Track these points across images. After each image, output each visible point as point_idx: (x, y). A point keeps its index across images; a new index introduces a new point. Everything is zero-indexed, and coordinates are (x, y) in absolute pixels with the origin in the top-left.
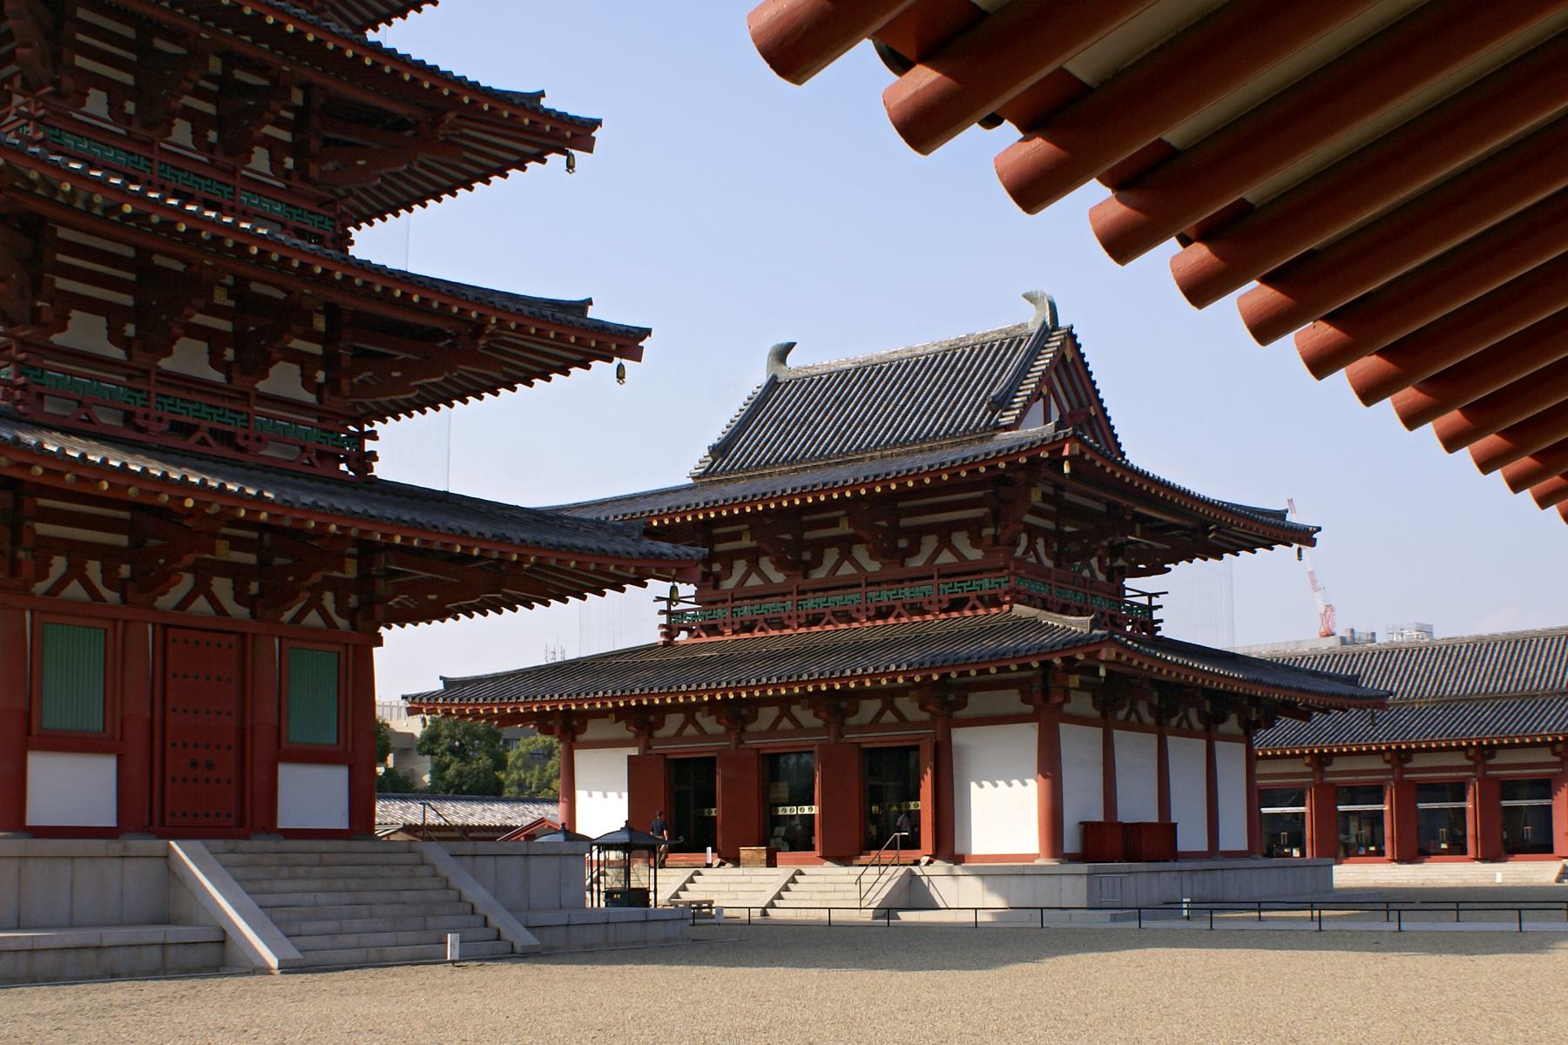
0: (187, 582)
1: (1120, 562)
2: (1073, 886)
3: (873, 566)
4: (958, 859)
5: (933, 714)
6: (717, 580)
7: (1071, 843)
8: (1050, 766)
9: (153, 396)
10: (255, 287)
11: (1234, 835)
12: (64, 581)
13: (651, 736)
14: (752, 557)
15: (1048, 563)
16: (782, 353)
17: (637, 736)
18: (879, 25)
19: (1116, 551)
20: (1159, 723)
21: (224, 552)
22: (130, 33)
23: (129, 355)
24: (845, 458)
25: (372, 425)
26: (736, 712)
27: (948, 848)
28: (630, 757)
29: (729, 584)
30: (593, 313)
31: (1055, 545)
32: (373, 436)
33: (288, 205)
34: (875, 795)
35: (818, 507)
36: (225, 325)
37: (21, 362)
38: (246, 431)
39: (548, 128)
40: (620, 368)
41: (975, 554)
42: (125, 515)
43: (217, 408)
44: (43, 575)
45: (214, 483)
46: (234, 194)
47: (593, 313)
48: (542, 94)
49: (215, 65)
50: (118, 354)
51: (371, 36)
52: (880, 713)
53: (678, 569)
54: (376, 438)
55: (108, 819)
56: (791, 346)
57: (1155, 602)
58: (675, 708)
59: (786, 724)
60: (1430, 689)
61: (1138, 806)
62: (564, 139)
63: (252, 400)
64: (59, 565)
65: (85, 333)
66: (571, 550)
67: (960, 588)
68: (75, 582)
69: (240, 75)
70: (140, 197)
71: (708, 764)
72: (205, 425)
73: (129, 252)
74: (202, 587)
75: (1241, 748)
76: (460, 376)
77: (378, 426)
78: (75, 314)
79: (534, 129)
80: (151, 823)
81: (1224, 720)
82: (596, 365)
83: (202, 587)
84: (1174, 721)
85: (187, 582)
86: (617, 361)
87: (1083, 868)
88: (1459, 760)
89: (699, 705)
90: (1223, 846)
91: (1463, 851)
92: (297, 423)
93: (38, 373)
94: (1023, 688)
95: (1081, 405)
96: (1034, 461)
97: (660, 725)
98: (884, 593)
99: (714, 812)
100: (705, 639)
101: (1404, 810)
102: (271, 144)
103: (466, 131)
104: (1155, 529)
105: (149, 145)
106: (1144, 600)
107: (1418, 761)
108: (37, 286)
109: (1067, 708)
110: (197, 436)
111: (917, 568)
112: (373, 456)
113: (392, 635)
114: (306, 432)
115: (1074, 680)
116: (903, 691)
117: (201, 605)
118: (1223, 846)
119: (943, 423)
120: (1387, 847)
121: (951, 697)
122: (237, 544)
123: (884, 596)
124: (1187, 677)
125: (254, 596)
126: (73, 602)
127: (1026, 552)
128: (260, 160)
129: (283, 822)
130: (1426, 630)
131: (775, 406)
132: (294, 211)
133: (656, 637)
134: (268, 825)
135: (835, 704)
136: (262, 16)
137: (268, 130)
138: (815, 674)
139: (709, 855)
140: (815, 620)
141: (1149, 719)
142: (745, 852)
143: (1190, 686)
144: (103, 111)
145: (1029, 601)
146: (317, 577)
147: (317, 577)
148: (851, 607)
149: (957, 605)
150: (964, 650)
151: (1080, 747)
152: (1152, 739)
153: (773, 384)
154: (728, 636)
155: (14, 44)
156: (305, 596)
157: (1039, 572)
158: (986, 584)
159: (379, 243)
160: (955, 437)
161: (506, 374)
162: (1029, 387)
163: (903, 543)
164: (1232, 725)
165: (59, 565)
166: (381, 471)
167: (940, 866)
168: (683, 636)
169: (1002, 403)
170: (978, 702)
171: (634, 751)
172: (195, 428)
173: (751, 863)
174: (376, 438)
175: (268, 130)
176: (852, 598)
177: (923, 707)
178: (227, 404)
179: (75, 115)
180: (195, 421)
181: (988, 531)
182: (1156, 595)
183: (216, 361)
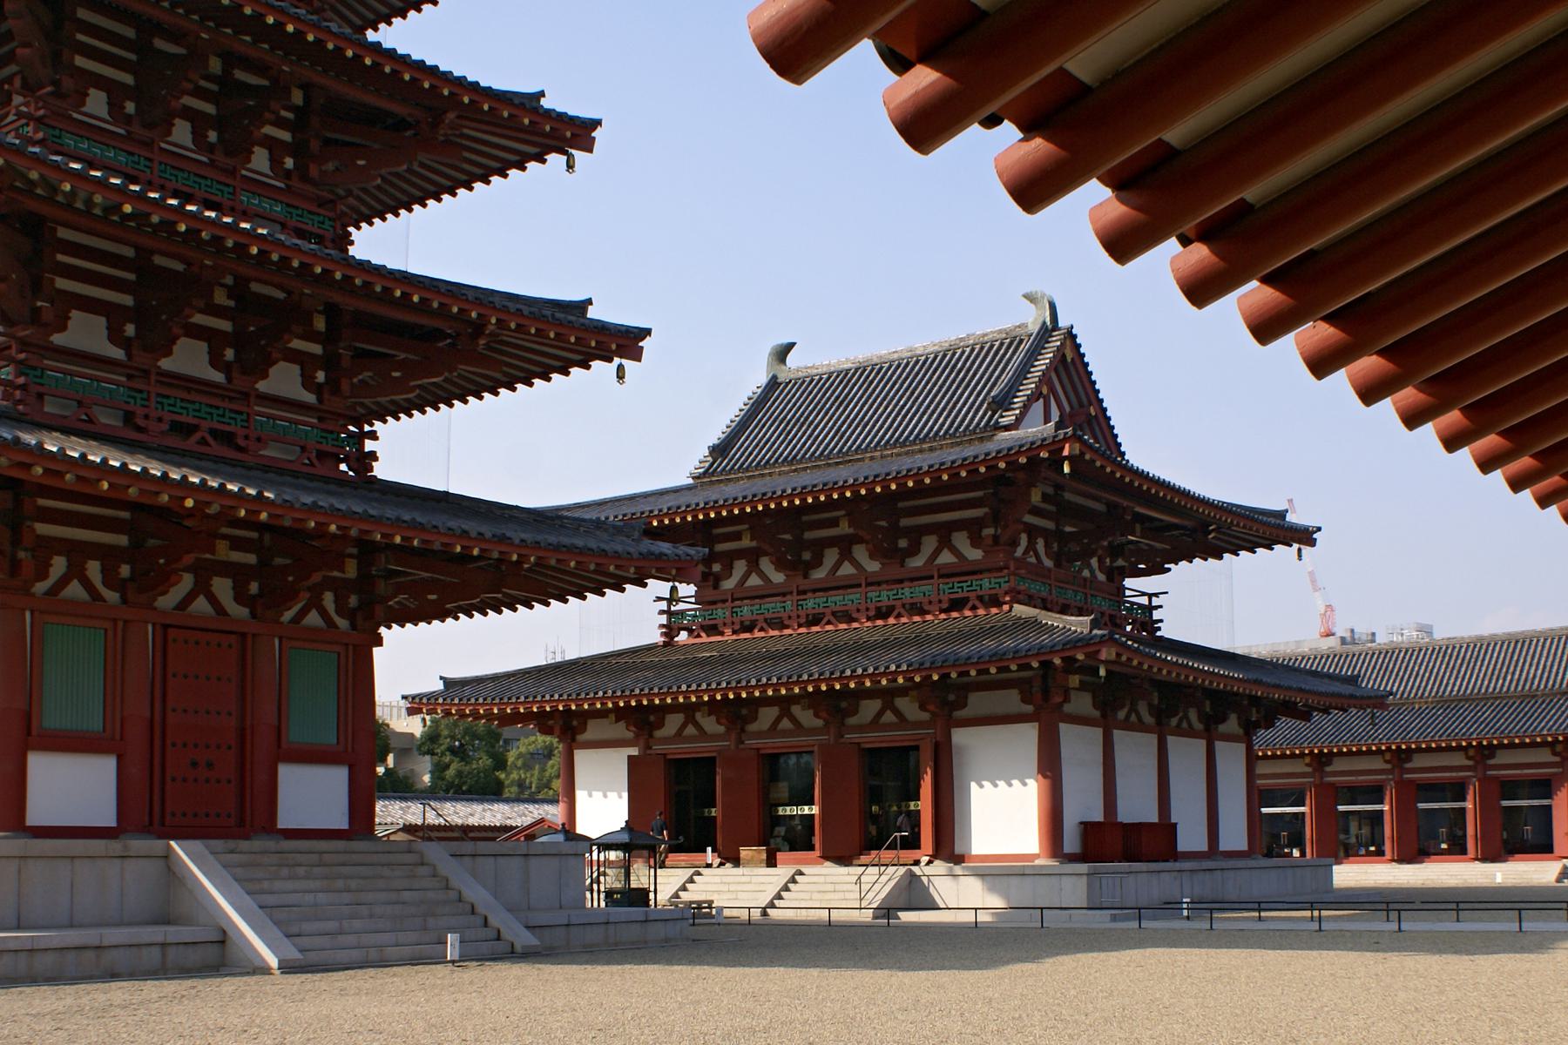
0: (187, 582)
1: (1120, 562)
2: (1073, 886)
3: (873, 566)
4: (958, 859)
5: (933, 714)
6: (717, 580)
7: (1071, 843)
8: (1050, 766)
9: (153, 396)
10: (255, 287)
11: (1234, 835)
12: (64, 581)
13: (651, 736)
14: (752, 557)
15: (1048, 563)
16: (782, 353)
17: (637, 736)
18: (879, 25)
19: (1116, 551)
20: (1159, 723)
21: (224, 552)
22: (130, 33)
23: (129, 355)
24: (845, 458)
25: (372, 425)
26: (736, 712)
27: (948, 848)
28: (630, 757)
29: (729, 584)
30: (593, 313)
31: (1055, 545)
32: (373, 436)
33: (288, 205)
34: (875, 795)
35: (818, 507)
36: (225, 325)
37: (21, 362)
38: (246, 431)
39: (548, 128)
40: (620, 368)
41: (975, 554)
42: (125, 515)
43: (217, 408)
44: (43, 575)
45: (214, 483)
46: (234, 194)
47: (593, 313)
48: (542, 94)
49: (215, 65)
50: (118, 354)
51: (371, 36)
52: (880, 713)
53: (678, 569)
54: (376, 438)
55: (108, 819)
56: (791, 346)
57: (1155, 602)
58: (675, 708)
59: (786, 724)
60: (1430, 689)
61: (1138, 806)
62: (564, 139)
63: (252, 400)
64: (59, 565)
65: (85, 333)
66: (571, 550)
67: (960, 588)
68: (75, 582)
69: (240, 75)
70: (140, 197)
71: (708, 764)
72: (205, 425)
73: (129, 252)
74: (202, 587)
75: (1241, 748)
76: (460, 376)
77: (378, 426)
78: (75, 314)
79: (534, 129)
80: (151, 823)
81: (1224, 720)
82: (596, 365)
83: (202, 587)
84: (1174, 721)
85: (187, 582)
86: (617, 361)
87: (1083, 868)
88: (1459, 760)
89: (699, 705)
90: (1223, 846)
91: (1463, 851)
92: (297, 423)
93: (38, 373)
94: (1023, 688)
95: (1081, 405)
96: (1034, 461)
97: (660, 725)
98: (884, 593)
99: (714, 812)
100: (705, 639)
101: (1404, 810)
102: (271, 144)
103: (466, 131)
104: (1155, 529)
105: (149, 145)
106: (1144, 600)
107: (1418, 761)
108: (37, 286)
109: (1067, 708)
110: (197, 436)
111: (917, 568)
112: (373, 456)
113: (392, 635)
114: (306, 432)
115: (1074, 680)
116: (903, 691)
117: (201, 605)
118: (1223, 846)
119: (943, 423)
120: (1387, 847)
121: (951, 697)
122: (237, 544)
123: (884, 596)
124: (1187, 677)
125: (254, 596)
126: (73, 602)
127: (1026, 552)
128: (260, 160)
129: (283, 822)
130: (1426, 630)
131: (775, 406)
132: (294, 211)
133: (656, 637)
134: (268, 825)
135: (835, 704)
136: (262, 16)
137: (268, 130)
138: (815, 674)
139: (709, 855)
140: (815, 620)
141: (1149, 719)
142: (745, 852)
143: (1190, 686)
144: (103, 111)
145: (1029, 601)
146: (317, 577)
147: (317, 577)
148: (851, 607)
149: (957, 605)
150: (964, 650)
151: (1080, 747)
152: (1152, 739)
153: (773, 384)
154: (728, 636)
155: (14, 44)
156: (305, 596)
157: (1039, 572)
158: (986, 584)
159: (379, 243)
160: (955, 437)
161: (506, 374)
162: (1029, 387)
163: (903, 543)
164: (1232, 725)
165: (59, 565)
166: (381, 471)
167: (940, 866)
168: (683, 636)
169: (1002, 403)
170: (978, 702)
171: (634, 751)
172: (195, 428)
173: (751, 863)
174: (376, 438)
175: (268, 130)
176: (852, 598)
177: (923, 707)
178: (227, 404)
179: (75, 115)
180: (195, 421)
181: (988, 531)
182: (1156, 595)
183: (216, 361)
